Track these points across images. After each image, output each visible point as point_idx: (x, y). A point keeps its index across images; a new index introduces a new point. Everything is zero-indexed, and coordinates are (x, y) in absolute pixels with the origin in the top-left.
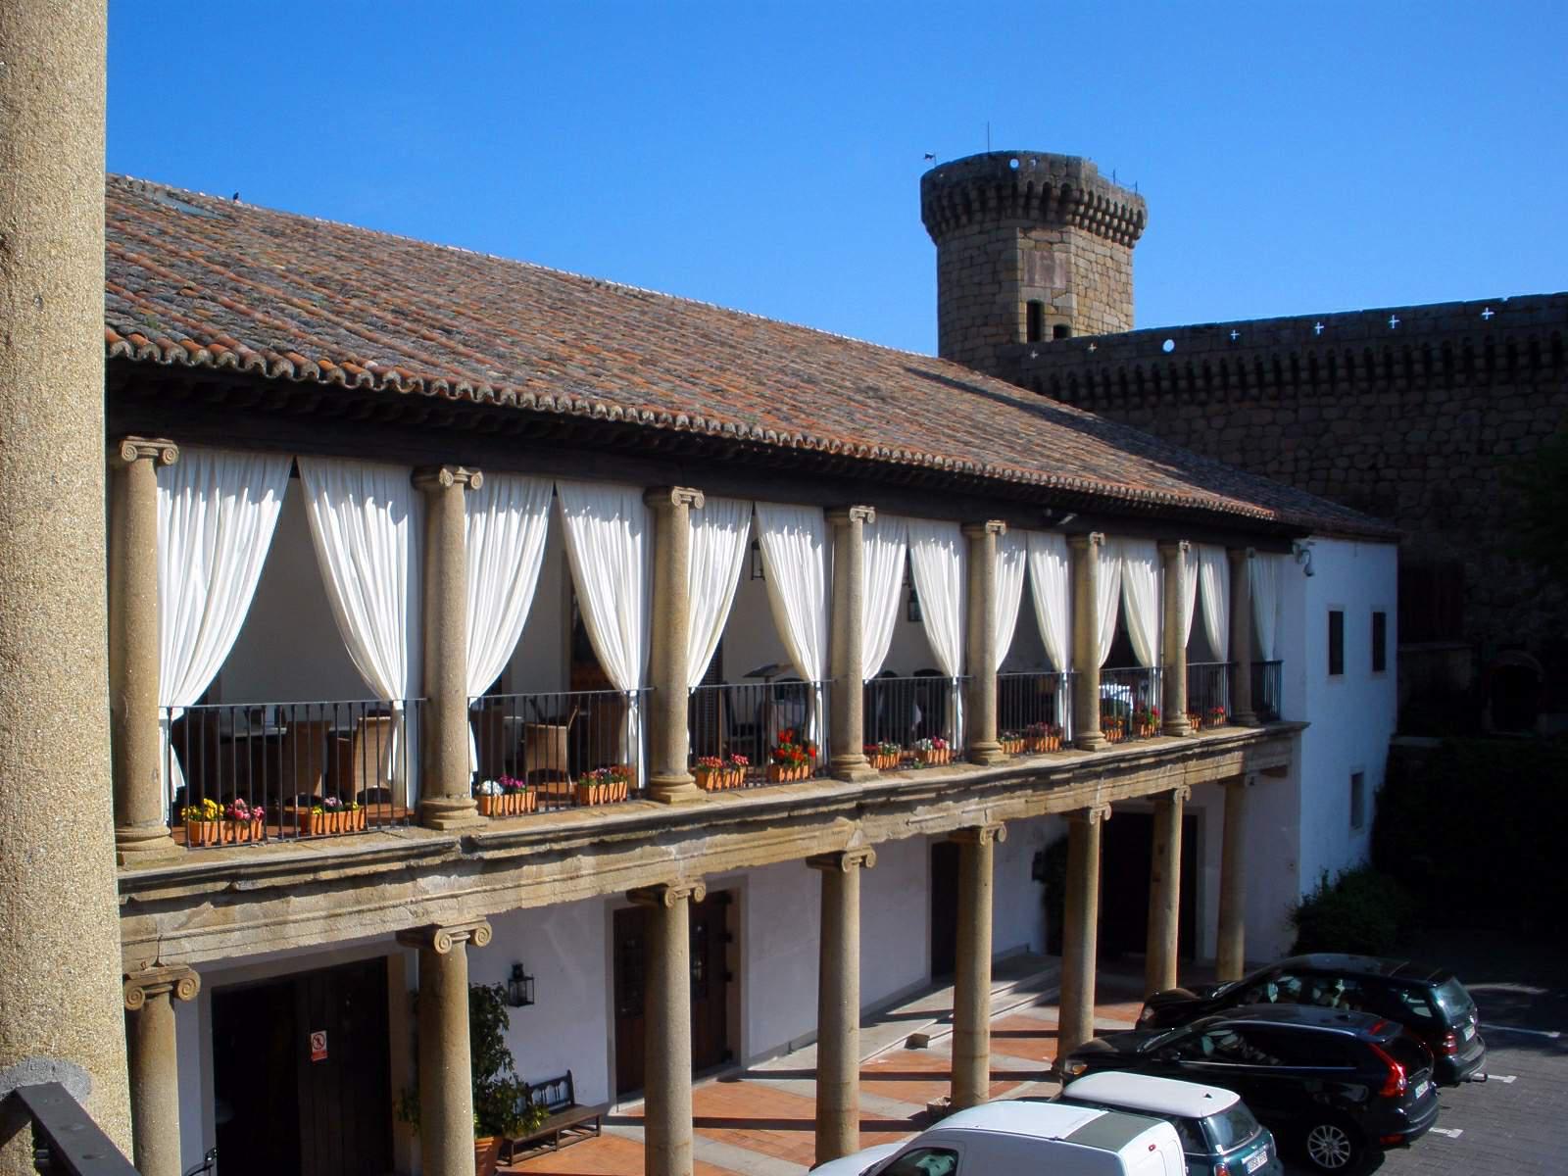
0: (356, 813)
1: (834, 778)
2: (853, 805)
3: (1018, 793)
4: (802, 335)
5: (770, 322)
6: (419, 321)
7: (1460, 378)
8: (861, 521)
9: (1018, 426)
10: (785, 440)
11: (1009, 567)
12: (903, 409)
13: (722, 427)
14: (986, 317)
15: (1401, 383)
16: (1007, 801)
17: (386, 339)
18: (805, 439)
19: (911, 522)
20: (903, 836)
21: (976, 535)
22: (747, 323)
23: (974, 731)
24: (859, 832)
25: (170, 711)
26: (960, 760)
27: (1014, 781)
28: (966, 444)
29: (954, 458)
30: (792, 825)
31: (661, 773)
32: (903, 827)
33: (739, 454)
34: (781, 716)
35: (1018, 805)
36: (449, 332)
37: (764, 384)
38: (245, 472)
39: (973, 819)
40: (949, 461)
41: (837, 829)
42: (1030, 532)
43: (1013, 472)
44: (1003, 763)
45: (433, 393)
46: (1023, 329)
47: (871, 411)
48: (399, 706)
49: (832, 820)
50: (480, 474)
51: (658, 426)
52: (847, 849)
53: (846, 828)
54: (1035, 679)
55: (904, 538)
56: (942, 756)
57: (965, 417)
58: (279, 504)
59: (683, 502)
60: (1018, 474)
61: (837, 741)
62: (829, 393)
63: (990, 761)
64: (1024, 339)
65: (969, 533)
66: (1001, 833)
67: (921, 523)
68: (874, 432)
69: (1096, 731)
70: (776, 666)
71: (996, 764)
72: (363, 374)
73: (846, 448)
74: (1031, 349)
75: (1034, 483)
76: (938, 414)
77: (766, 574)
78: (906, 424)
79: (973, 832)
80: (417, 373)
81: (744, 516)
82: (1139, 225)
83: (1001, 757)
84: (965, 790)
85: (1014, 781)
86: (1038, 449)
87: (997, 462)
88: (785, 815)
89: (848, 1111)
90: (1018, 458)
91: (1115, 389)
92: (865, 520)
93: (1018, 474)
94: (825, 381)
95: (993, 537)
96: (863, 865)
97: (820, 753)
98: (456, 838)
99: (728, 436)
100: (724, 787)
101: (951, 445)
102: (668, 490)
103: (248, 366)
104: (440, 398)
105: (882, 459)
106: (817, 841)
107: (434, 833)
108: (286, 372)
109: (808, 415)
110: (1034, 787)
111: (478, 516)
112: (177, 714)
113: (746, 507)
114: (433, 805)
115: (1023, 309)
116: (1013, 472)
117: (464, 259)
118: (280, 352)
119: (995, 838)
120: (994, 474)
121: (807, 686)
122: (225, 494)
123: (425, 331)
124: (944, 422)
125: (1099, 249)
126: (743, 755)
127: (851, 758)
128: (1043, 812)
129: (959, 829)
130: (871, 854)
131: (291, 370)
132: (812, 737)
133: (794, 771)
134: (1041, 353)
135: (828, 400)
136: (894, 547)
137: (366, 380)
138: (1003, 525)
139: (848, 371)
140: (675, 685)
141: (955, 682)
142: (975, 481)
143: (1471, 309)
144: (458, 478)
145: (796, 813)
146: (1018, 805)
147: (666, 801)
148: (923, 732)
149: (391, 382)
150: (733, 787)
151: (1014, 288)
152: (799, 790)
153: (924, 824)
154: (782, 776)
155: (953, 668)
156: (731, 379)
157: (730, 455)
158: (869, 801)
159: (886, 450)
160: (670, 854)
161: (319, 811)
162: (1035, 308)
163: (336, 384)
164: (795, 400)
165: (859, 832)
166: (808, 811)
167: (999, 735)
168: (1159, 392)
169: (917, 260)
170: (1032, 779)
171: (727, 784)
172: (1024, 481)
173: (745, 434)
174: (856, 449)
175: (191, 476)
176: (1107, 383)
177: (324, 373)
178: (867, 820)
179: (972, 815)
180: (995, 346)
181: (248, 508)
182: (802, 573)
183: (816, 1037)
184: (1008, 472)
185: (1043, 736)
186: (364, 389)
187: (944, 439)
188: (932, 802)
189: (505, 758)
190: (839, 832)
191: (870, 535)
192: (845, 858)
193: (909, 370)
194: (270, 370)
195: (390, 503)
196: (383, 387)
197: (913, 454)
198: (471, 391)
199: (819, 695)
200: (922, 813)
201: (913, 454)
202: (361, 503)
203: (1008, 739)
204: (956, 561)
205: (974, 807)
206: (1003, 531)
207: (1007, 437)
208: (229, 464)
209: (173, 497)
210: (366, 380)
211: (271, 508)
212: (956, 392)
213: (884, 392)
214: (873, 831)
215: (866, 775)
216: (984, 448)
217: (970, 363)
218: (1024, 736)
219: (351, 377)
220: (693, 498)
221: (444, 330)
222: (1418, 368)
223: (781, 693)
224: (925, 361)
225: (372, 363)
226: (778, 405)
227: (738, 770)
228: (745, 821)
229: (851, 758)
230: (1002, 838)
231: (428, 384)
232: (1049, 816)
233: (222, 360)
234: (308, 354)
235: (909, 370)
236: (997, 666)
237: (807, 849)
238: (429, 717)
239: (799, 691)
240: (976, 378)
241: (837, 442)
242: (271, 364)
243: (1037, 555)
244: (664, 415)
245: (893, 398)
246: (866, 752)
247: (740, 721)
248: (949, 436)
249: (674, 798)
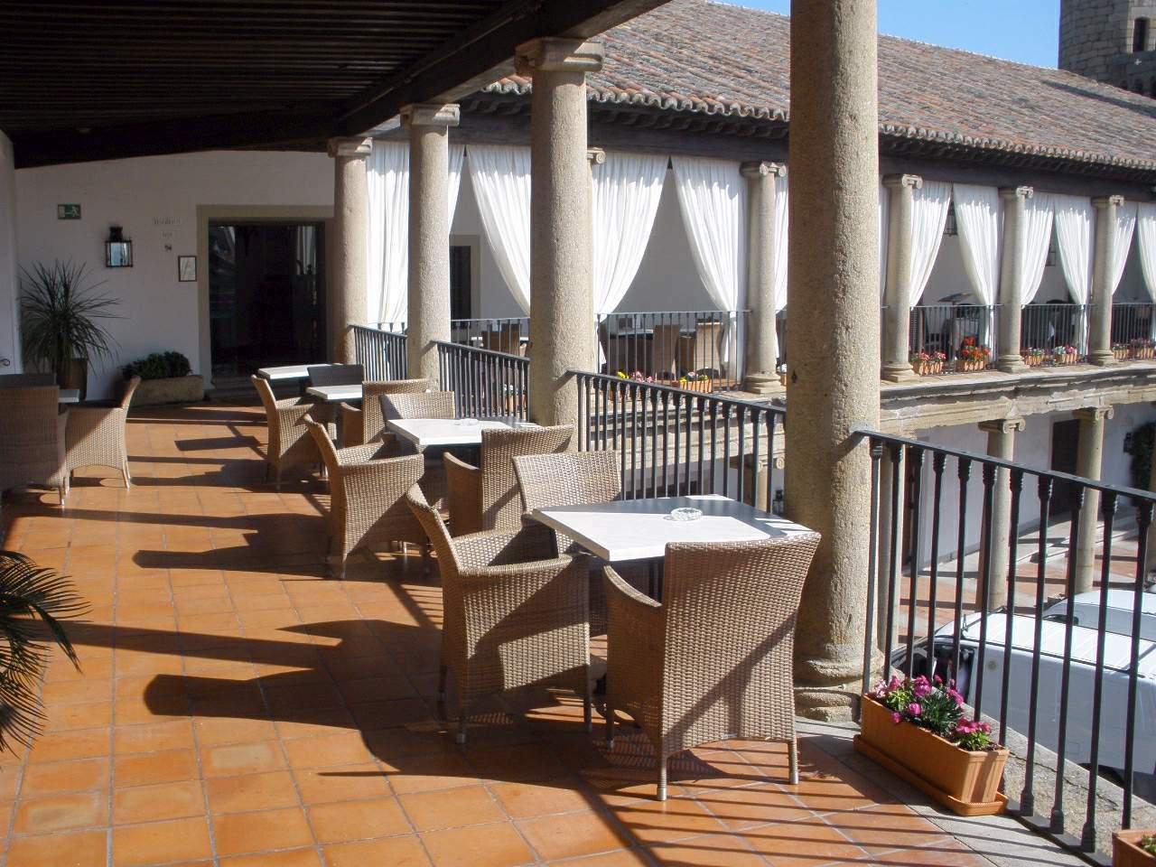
0: (707, 381)
1: (1000, 370)
2: (1012, 388)
3: (1123, 386)
4: (964, 58)
5: (939, 48)
6: (729, 64)
8: (1023, 197)
9: (1131, 124)
10: (977, 143)
11: (1122, 230)
12: (1048, 116)
13: (937, 135)
14: (1100, 34)
16: (1115, 392)
17: (718, 79)
18: (990, 141)
19: (1056, 198)
20: (1043, 412)
21: (1102, 206)
22: (925, 51)
23: (1095, 343)
24: (1014, 408)
25: (599, 316)
26: (991, 368)
27: (1121, 378)
28: (1096, 140)
29: (1091, 152)
30: (972, 400)
31: (891, 362)
32: (1044, 406)
33: (947, 152)
34: (962, 328)
35: (1123, 394)
36: (750, 71)
37: (952, 101)
38: (641, 167)
39: (1091, 403)
40: (1087, 155)
41: (1000, 405)
42: (1140, 203)
43: (1133, 161)
44: (1115, 364)
45: (760, 116)
46: (1130, 42)
47: (1027, 118)
48: (733, 315)
49: (998, 398)
50: (784, 167)
51: (897, 135)
52: (1006, 418)
53: (1007, 404)
54: (1133, 309)
55: (1052, 208)
56: (1071, 358)
57: (1092, 119)
58: (661, 187)
59: (909, 184)
60: (1136, 162)
61: (1003, 347)
62: (995, 105)
63: (1106, 363)
64: (1130, 49)
65: (1096, 205)
66: (1109, 413)
67: (1064, 198)
68: (1032, 134)
70: (960, 295)
71: (1108, 366)
72: (718, 106)
73: (1017, 147)
74: (1136, 57)
75: (1147, 168)
76: (1072, 118)
77: (959, 231)
78: (1052, 127)
79: (1091, 411)
80: (750, 106)
81: (946, 194)
83: (1113, 360)
84: (1087, 382)
85: (1121, 378)
86: (1149, 142)
87: (1120, 154)
88: (969, 393)
89: (998, 594)
90: (1135, 150)
92: (1026, 196)
93: (1136, 162)
94: (991, 95)
95: (1114, 207)
96: (1016, 429)
97: (991, 354)
98: (769, 399)
99: (940, 141)
100: (930, 373)
101: (1086, 143)
102: (900, 176)
103: (650, 102)
104: (764, 120)
105: (1041, 154)
106: (987, 411)
107: (755, 395)
108: (673, 105)
109: (987, 123)
110: (1135, 383)
111: (781, 193)
112: (603, 318)
113: (948, 186)
114: (753, 379)
115: (1131, 25)
116: (1133, 161)
117: (729, 11)
118: (667, 92)
119: (1106, 417)
120: (1132, 165)
121: (984, 308)
122: (629, 181)
123: (737, 72)
124: (1078, 125)
126: (943, 352)
127: (1010, 357)
128: (1140, 400)
129: (1081, 409)
130: (1022, 422)
131: (676, 104)
132: (986, 343)
133: (974, 365)
134: (1144, 60)
135: (996, 111)
136: (1046, 214)
137: (720, 109)
138: (1122, 199)
139: (1003, 87)
140: (902, 304)
141: (1082, 308)
142: (1105, 168)
144: (771, 170)
145: (976, 392)
146: (1123, 394)
147: (895, 380)
148: (1057, 341)
149: (735, 109)
150: (935, 373)
151: (1126, 10)
152: (978, 377)
153: (1058, 404)
154: (966, 367)
155: (1082, 298)
156: (930, 98)
157: (940, 154)
158: (1023, 386)
159: (1044, 148)
160: (895, 415)
161: (684, 380)
163: (701, 113)
164: (975, 112)
165: (1014, 408)
166: (983, 391)
167: (1112, 347)
170: (1134, 377)
171: (932, 372)
172: (1140, 168)
173: (952, 139)
174: (1024, 148)
175: (609, 172)
177: (695, 105)
178: (1021, 399)
179: (1091, 400)
180: (1105, 56)
181: (643, 189)
182: (983, 233)
183: (978, 547)
184: (1129, 161)
185: (1143, 347)
186: (718, 115)
187: (1081, 138)
188: (1064, 389)
189: (1031, 340)
190: (1001, 407)
191: (1029, 206)
192: (1005, 424)
193: (1044, 82)
194: (663, 105)
195: (728, 186)
196: (730, 113)
197: (1062, 151)
198: (783, 114)
199: (992, 314)
200: (1056, 396)
201: (1062, 151)
202: (710, 185)
203: (1117, 348)
204: (1087, 224)
205: (1092, 395)
206: (1122, 203)
207: (1124, 133)
208: (631, 162)
209: (599, 183)
210: (720, 109)
211: (656, 189)
212: (1081, 98)
213: (1032, 102)
214: (1024, 407)
215: (1021, 369)
216: (1110, 144)
217: (1084, 71)
218: (1128, 348)
219: (711, 107)
220: (916, 181)
221: (748, 71)
223: (960, 312)
224: (1053, 74)
225: (721, 98)
226: (966, 117)
227: (939, 363)
228: (943, 396)
229: (1010, 357)
230: (1111, 417)
231: (757, 111)
232: (1144, 404)
233: (635, 99)
234: (682, 92)
235: (1044, 82)
236: (1113, 292)
237: (981, 416)
238: (751, 323)
239: (976, 312)
240: (1092, 86)
241: (1011, 144)
242: (664, 101)
243: (1145, 220)
244: (901, 128)
245: (1039, 107)
246: (1021, 354)
247: (931, 332)
248: (1083, 135)
249: (900, 378)
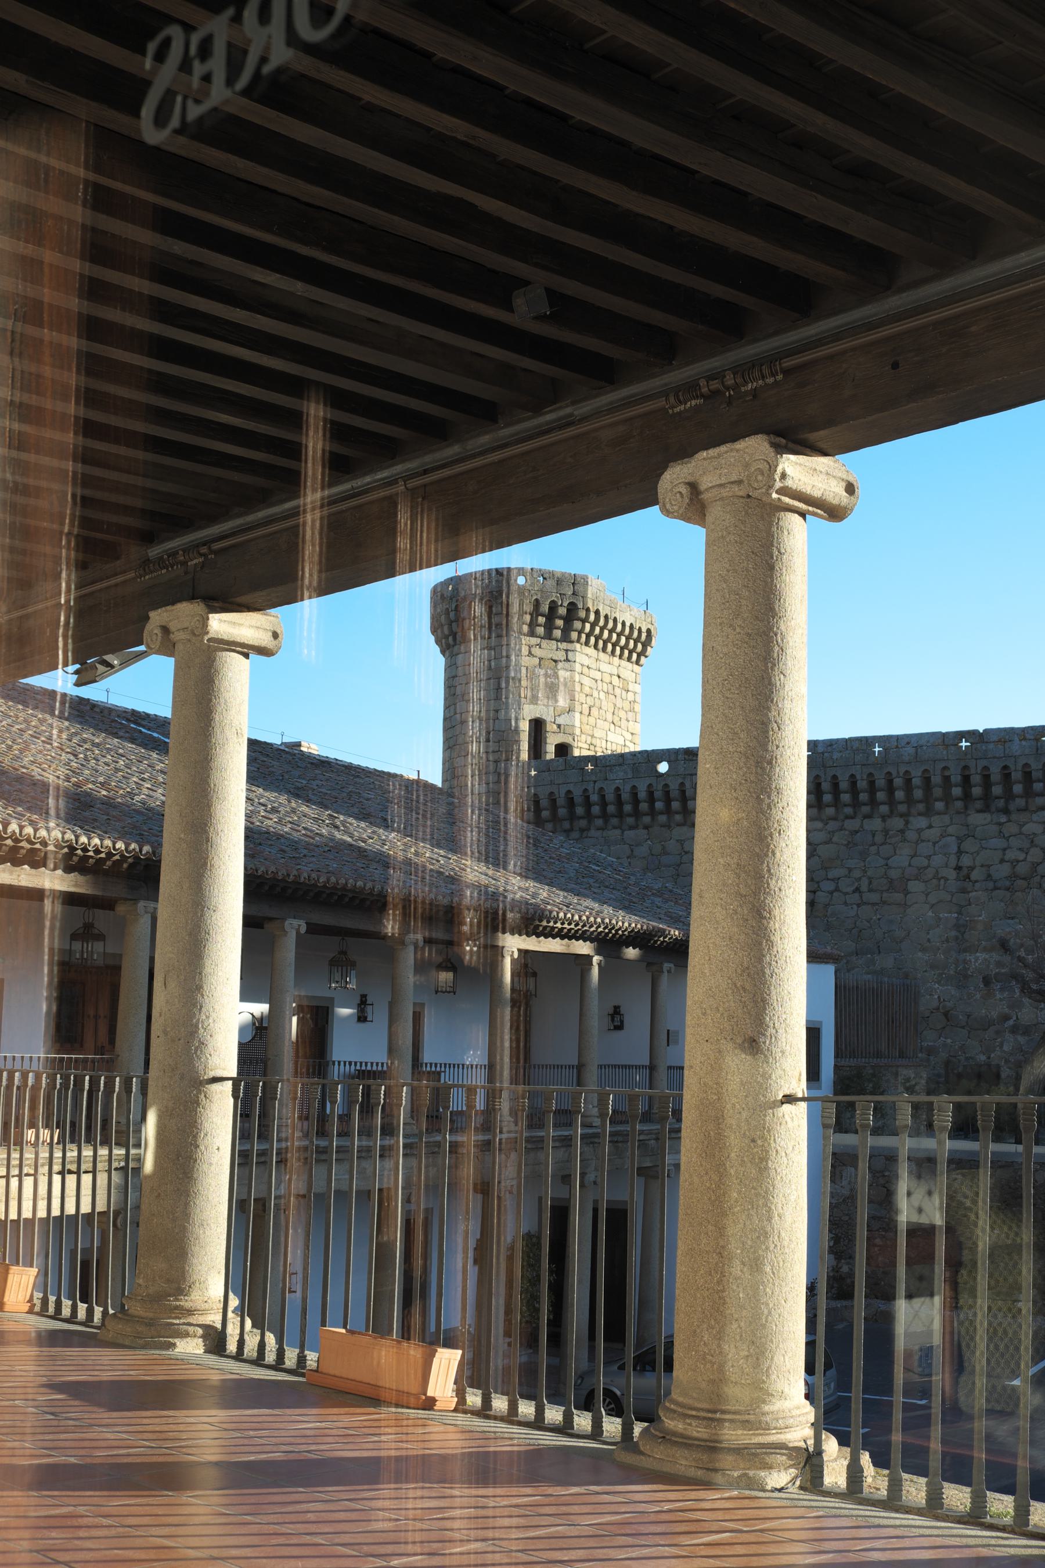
7: (939, 805)
15: (884, 809)
46: (525, 746)
82: (647, 643)
91: (611, 809)
115: (525, 726)
125: (604, 667)
143: (867, 742)
162: (538, 726)
176: (604, 804)
222: (900, 795)
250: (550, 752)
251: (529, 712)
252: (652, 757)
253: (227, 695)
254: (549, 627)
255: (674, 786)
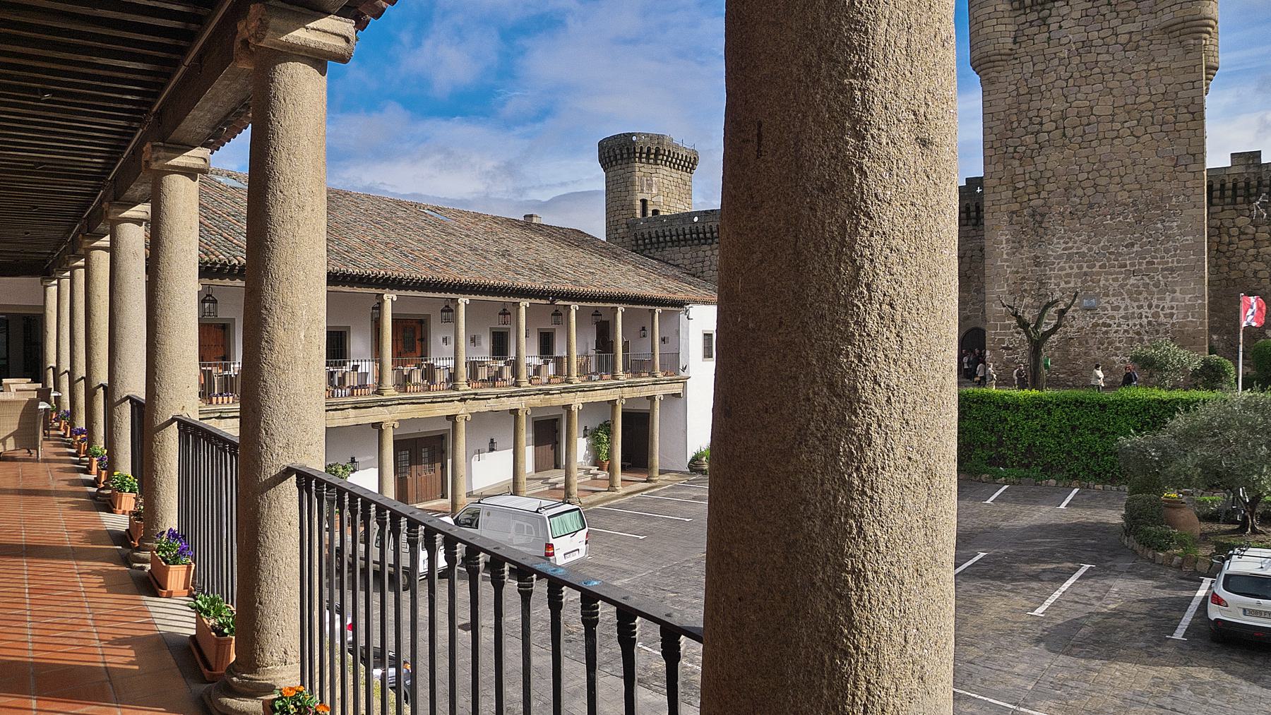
64: (639, 216)
69: (574, 374)
82: (694, 164)
115: (638, 203)
162: (644, 202)
168: (679, 240)
169: (594, 178)
250: (650, 213)
251: (640, 196)
252: (691, 215)
253: (269, 543)
254: (648, 158)
255: (700, 227)
